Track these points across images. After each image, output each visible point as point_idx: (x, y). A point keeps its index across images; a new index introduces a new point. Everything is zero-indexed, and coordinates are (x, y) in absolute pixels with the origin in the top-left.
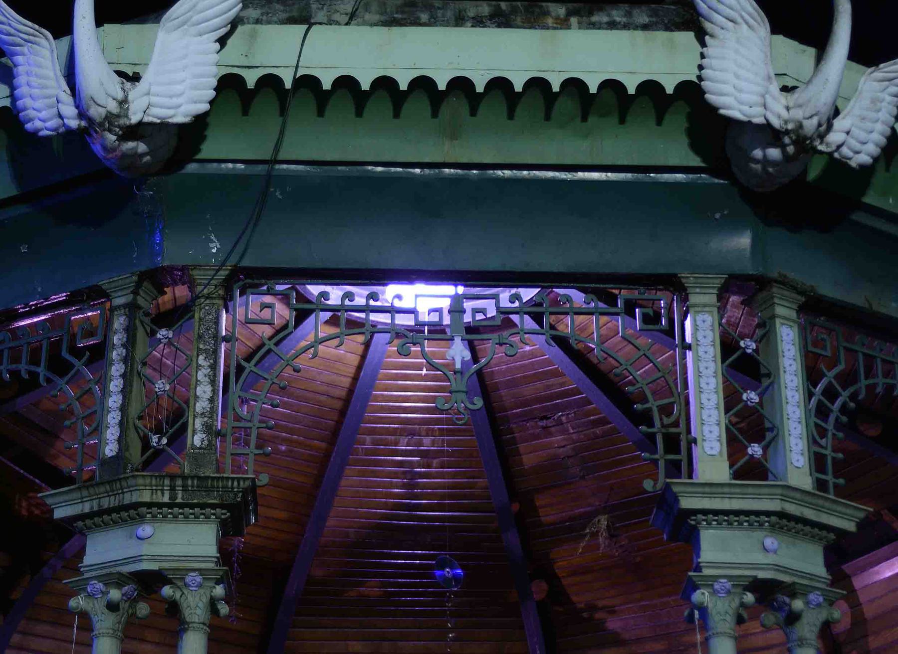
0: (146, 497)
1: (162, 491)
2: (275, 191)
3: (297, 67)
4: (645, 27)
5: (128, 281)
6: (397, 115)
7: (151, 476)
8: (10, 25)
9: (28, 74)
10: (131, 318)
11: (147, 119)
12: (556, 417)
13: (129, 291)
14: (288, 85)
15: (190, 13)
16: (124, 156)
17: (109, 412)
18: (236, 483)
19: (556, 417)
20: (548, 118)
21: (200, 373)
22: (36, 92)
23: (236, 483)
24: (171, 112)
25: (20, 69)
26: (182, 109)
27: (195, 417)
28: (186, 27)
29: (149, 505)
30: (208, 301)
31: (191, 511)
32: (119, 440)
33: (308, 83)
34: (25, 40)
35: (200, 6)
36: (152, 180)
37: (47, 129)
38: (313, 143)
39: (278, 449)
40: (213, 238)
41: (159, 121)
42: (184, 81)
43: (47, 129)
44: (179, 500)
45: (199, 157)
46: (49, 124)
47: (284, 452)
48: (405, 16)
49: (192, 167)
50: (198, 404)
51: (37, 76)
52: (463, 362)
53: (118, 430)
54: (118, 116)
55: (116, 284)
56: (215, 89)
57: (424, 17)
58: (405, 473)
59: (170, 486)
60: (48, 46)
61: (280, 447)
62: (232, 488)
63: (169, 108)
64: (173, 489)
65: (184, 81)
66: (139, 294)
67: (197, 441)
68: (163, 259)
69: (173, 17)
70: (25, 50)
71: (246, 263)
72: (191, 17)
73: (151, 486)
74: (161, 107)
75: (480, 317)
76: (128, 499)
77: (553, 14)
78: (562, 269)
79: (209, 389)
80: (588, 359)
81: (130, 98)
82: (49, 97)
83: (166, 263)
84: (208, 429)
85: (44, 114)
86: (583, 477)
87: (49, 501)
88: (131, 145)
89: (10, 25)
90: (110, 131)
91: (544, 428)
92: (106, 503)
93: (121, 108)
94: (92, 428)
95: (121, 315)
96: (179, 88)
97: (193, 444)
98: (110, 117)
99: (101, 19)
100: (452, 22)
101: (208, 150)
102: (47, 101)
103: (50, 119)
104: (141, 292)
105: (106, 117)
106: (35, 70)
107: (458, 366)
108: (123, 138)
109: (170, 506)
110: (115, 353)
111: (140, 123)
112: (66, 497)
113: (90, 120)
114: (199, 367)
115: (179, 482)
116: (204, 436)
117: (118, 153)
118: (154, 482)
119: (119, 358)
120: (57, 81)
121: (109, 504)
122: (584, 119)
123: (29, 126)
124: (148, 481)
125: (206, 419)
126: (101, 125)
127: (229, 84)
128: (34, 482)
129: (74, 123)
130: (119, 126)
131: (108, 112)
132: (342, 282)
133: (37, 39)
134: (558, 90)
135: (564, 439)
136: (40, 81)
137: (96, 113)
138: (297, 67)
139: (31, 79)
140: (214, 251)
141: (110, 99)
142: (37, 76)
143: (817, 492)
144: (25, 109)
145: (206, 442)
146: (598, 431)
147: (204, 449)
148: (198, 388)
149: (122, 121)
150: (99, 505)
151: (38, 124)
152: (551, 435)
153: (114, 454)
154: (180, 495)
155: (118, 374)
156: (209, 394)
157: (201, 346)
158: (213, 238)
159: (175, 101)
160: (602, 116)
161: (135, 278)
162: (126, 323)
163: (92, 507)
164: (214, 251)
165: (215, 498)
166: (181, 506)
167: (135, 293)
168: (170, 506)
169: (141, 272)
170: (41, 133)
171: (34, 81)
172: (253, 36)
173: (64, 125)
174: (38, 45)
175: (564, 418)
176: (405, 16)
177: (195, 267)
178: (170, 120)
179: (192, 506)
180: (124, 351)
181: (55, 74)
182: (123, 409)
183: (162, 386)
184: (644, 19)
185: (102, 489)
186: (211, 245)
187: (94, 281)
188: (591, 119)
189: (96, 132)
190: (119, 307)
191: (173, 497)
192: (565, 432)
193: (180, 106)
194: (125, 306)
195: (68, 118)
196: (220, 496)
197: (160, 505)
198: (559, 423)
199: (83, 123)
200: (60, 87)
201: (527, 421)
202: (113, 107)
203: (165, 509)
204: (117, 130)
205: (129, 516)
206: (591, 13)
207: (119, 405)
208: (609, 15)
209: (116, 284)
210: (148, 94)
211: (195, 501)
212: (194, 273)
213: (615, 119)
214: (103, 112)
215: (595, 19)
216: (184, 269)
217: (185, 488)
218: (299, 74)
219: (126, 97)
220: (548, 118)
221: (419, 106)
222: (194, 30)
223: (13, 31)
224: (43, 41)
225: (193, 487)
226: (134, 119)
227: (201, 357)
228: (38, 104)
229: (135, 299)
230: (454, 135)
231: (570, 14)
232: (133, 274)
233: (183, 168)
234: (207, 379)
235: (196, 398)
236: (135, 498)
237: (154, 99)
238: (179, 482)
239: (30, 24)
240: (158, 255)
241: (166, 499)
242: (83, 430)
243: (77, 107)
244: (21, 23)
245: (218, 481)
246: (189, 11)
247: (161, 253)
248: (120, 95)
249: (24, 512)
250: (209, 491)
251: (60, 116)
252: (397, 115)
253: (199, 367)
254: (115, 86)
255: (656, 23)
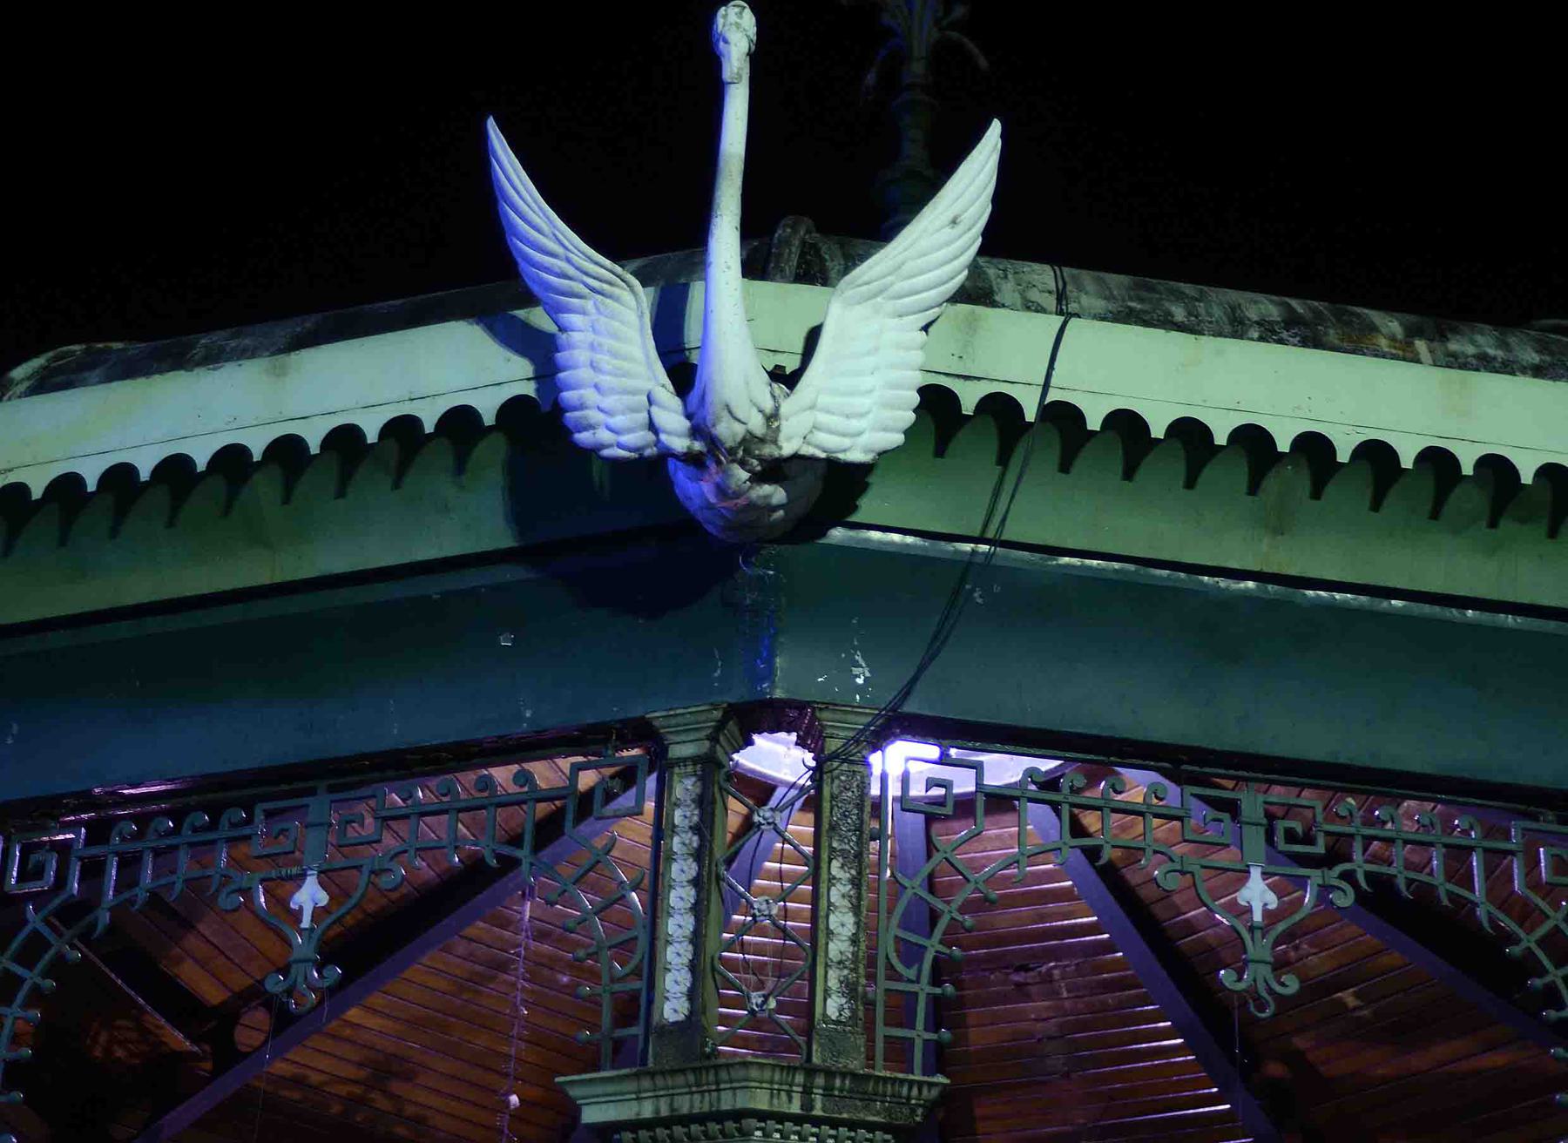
0: (761, 1102)
1: (789, 1093)
2: (973, 590)
3: (1046, 386)
4: (1538, 371)
5: (703, 717)
6: (1190, 483)
7: (774, 1066)
8: (568, 261)
9: (592, 347)
10: (705, 780)
11: (808, 450)
12: (1044, 969)
13: (703, 734)
14: (1030, 415)
15: (890, 278)
16: (751, 506)
17: (668, 943)
18: (915, 1092)
19: (1044, 969)
20: (1435, 514)
21: (833, 891)
22: (606, 380)
23: (915, 1092)
24: (847, 442)
25: (576, 336)
26: (865, 439)
27: (827, 965)
28: (879, 299)
29: (762, 1116)
30: (845, 767)
31: (814, 1130)
32: (692, 994)
33: (1063, 416)
34: (593, 290)
35: (906, 269)
36: (773, 550)
37: (620, 446)
38: (1070, 521)
39: (557, 982)
40: (858, 658)
41: (823, 455)
42: (871, 391)
43: (620, 446)
44: (818, 1112)
45: (854, 518)
46: (626, 439)
47: (566, 986)
48: (1147, 307)
49: (838, 534)
50: (831, 946)
51: (614, 354)
52: (1267, 913)
53: (689, 976)
54: (762, 440)
55: (680, 720)
56: (915, 411)
57: (1332, 336)
58: (761, 1040)
59: (804, 1086)
60: (633, 303)
61: (559, 976)
62: (909, 1098)
63: (844, 435)
64: (807, 1092)
65: (871, 391)
66: (718, 741)
67: (832, 1012)
68: (773, 685)
69: (866, 278)
70: (589, 305)
71: (910, 707)
72: (892, 284)
73: (772, 1082)
74: (831, 432)
75: (938, 792)
76: (727, 1102)
77: (1384, 330)
78: (1428, 770)
79: (850, 919)
80: (1122, 877)
81: (783, 410)
82: (634, 393)
83: (779, 694)
84: (850, 989)
85: (618, 421)
86: (1067, 1075)
87: (574, 1092)
88: (767, 489)
89: (568, 261)
90: (743, 464)
91: (1018, 985)
92: (684, 1105)
93: (769, 427)
94: (628, 969)
95: (687, 776)
96: (864, 402)
97: (824, 1014)
98: (750, 441)
99: (754, 267)
100: (1228, 329)
101: (868, 508)
102: (628, 400)
103: (630, 430)
104: (722, 738)
105: (744, 440)
106: (608, 342)
107: (1258, 917)
108: (758, 478)
109: (798, 1120)
110: (676, 840)
111: (796, 457)
112: (610, 1088)
113: (713, 442)
114: (832, 880)
115: (820, 1080)
116: (844, 1000)
117: (741, 502)
118: (777, 1077)
119: (685, 850)
120: (650, 366)
121: (692, 1107)
122: (1493, 524)
123: (583, 437)
124: (767, 1074)
125: (846, 972)
126: (731, 452)
127: (936, 403)
128: (137, 1002)
129: (680, 444)
130: (761, 459)
131: (748, 432)
132: (1025, 750)
133: (616, 291)
134: (1224, 443)
135: (1048, 1008)
136: (615, 362)
137: (728, 431)
138: (1046, 386)
139: (599, 356)
140: (860, 681)
141: (754, 411)
142: (614, 354)
143: (642, 1021)
144: (582, 407)
145: (847, 1013)
146: (1110, 998)
147: (844, 1024)
148: (832, 917)
149: (768, 450)
150: (671, 1104)
151: (604, 436)
152: (1028, 998)
153: (681, 1017)
154: (818, 1104)
155: (684, 878)
156: (850, 929)
157: (835, 844)
158: (858, 658)
159: (855, 424)
160: (1523, 521)
161: (717, 714)
162: (698, 790)
163: (657, 1111)
164: (860, 681)
165: (878, 1114)
166: (817, 1122)
167: (714, 739)
168: (798, 1120)
169: (730, 705)
170: (606, 452)
171: (604, 360)
172: (971, 326)
173: (658, 442)
174: (610, 296)
175: (1056, 972)
176: (1147, 307)
177: (828, 706)
178: (841, 456)
179: (834, 1124)
180: (695, 838)
181: (647, 356)
182: (697, 939)
183: (764, 906)
184: (1533, 357)
185: (680, 1079)
186: (856, 671)
187: (636, 712)
188: (1506, 525)
189: (719, 462)
190: (683, 761)
191: (807, 1105)
192: (1055, 994)
193: (859, 434)
194: (695, 760)
195: (669, 433)
196: (886, 1110)
197: (781, 1118)
198: (1048, 978)
199: (698, 446)
200: (656, 378)
201: (992, 971)
202: (757, 424)
203: (788, 1125)
204: (755, 462)
205: (722, 1132)
206: (1443, 337)
207: (688, 933)
208: (1473, 342)
209: (680, 720)
210: (812, 407)
211: (845, 1116)
212: (825, 715)
213: (1543, 530)
214: (740, 430)
215: (1453, 346)
216: (801, 706)
217: (828, 1091)
218: (1048, 400)
219: (777, 408)
220: (1435, 514)
221: (1230, 476)
222: (891, 306)
223: (571, 271)
224: (626, 295)
225: (841, 1090)
226: (787, 448)
227: (835, 864)
228: (609, 402)
229: (712, 750)
230: (1278, 526)
231: (1413, 332)
232: (715, 707)
233: (824, 534)
234: (846, 903)
235: (830, 934)
236: (742, 1101)
237: (823, 418)
238: (820, 1080)
239: (607, 263)
240: (763, 680)
241: (795, 1108)
242: (612, 967)
243: (689, 416)
244: (597, 263)
245: (773, 1071)
246: (890, 274)
247: (770, 674)
248: (768, 406)
249: (98, 1053)
250: (868, 1099)
251: (652, 427)
252: (1190, 483)
253: (832, 880)
254: (763, 392)
255: (1552, 365)
